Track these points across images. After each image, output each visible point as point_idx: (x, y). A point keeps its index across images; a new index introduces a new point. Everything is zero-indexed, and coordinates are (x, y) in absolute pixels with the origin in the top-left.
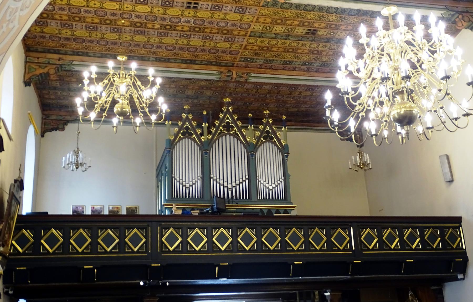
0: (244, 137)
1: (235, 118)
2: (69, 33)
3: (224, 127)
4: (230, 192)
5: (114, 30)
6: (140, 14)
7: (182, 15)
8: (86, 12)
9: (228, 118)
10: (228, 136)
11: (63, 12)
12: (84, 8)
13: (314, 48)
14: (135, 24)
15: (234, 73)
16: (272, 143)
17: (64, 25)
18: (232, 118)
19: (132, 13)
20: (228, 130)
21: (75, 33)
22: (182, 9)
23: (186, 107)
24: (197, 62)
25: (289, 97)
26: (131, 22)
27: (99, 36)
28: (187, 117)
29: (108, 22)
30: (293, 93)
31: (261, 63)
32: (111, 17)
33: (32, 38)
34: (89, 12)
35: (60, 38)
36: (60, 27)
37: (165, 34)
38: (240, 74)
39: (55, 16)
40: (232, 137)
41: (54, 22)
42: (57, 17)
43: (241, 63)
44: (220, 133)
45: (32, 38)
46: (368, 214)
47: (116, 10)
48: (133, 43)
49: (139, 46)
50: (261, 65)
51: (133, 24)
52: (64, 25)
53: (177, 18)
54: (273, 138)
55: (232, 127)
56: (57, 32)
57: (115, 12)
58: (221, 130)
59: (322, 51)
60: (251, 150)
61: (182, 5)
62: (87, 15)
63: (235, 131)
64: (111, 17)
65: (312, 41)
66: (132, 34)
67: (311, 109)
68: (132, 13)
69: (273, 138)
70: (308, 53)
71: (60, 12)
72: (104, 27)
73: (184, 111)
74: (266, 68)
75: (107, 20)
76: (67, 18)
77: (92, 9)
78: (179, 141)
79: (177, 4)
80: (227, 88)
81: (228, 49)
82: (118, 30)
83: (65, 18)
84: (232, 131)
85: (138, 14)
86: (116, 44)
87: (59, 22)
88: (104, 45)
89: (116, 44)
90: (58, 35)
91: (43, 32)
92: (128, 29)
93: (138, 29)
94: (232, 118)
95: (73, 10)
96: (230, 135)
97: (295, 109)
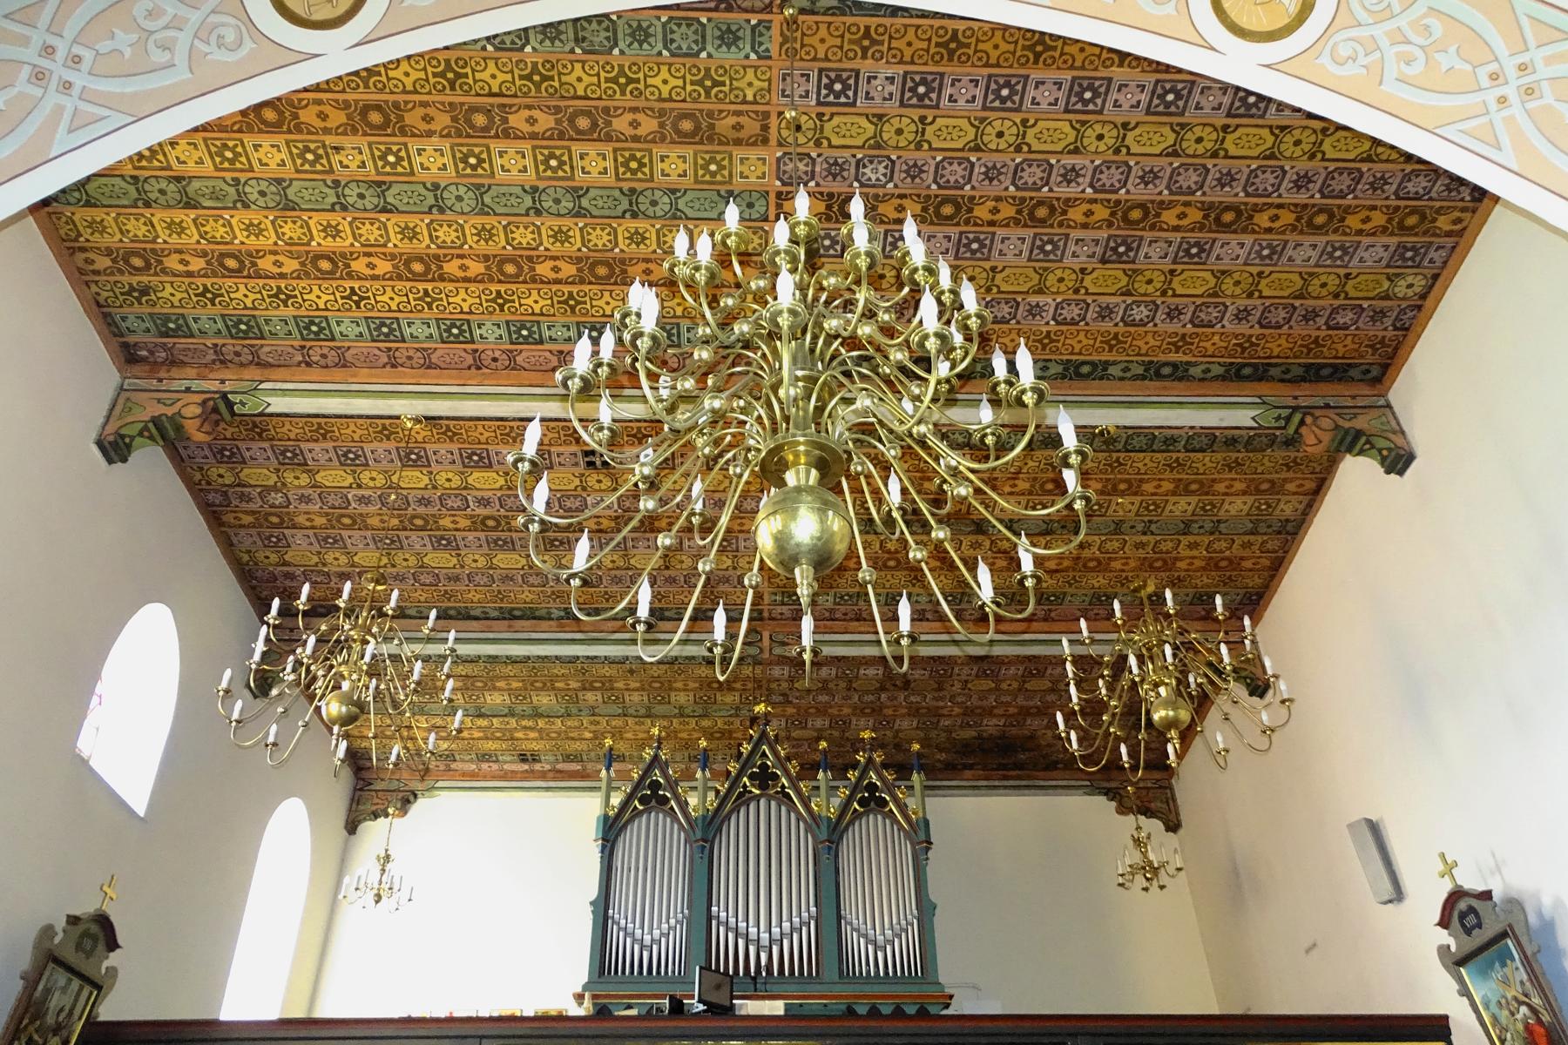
0: (903, 808)
1: (782, 753)
2: (343, 560)
3: (752, 777)
4: (646, 954)
5: (439, 542)
6: (487, 494)
7: (584, 489)
8: (361, 499)
9: (764, 754)
10: (763, 802)
11: (310, 507)
12: (354, 492)
13: (1221, 551)
14: (483, 522)
15: (766, 635)
16: (666, 814)
17: (325, 540)
18: (776, 754)
19: (464, 493)
20: (763, 787)
21: (356, 559)
22: (577, 471)
23: (866, 735)
24: (667, 614)
25: (941, 699)
26: (472, 516)
27: (413, 561)
28: (870, 761)
29: (419, 522)
30: (947, 686)
31: (830, 605)
32: (421, 510)
33: (268, 581)
34: (364, 500)
35: (328, 574)
36: (316, 547)
37: (562, 543)
38: (781, 637)
39: (369, 521)
40: (773, 803)
41: (299, 533)
42: (301, 520)
43: (779, 609)
44: (741, 795)
45: (268, 581)
46: (1215, 1010)
47: (426, 488)
48: (497, 574)
49: (728, 581)
50: (831, 611)
51: (480, 524)
52: (325, 540)
53: (575, 497)
54: (885, 803)
55: (776, 777)
56: (316, 559)
57: (427, 494)
58: (745, 786)
59: (1242, 559)
60: (830, 836)
61: (574, 460)
62: (363, 509)
63: (783, 787)
64: (421, 510)
65: (1212, 533)
66: (485, 550)
67: (1014, 731)
68: (464, 493)
69: (667, 800)
70: (1204, 569)
71: (303, 507)
72: (414, 536)
73: (857, 745)
74: (845, 618)
75: (414, 517)
76: (324, 520)
77: (369, 492)
78: (851, 822)
79: (561, 459)
80: (769, 681)
81: (731, 572)
82: (445, 542)
83: (320, 521)
84: (775, 786)
85: (479, 494)
86: (457, 579)
87: (311, 532)
88: (431, 585)
89: (457, 579)
90: (320, 567)
91: (285, 564)
92: (471, 536)
93: (494, 535)
94: (776, 754)
95: (331, 499)
96: (769, 798)
97: (969, 734)
